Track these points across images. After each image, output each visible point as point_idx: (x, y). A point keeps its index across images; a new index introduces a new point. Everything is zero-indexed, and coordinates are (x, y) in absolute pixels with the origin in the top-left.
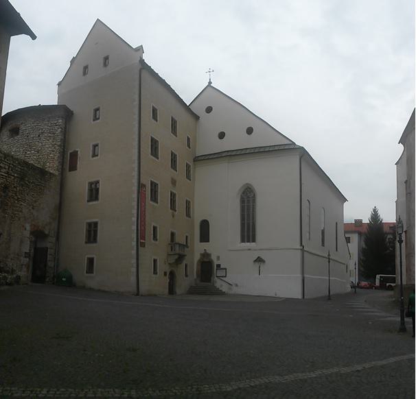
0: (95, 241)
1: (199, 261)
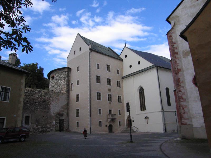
0: (79, 116)
1: (127, 120)
